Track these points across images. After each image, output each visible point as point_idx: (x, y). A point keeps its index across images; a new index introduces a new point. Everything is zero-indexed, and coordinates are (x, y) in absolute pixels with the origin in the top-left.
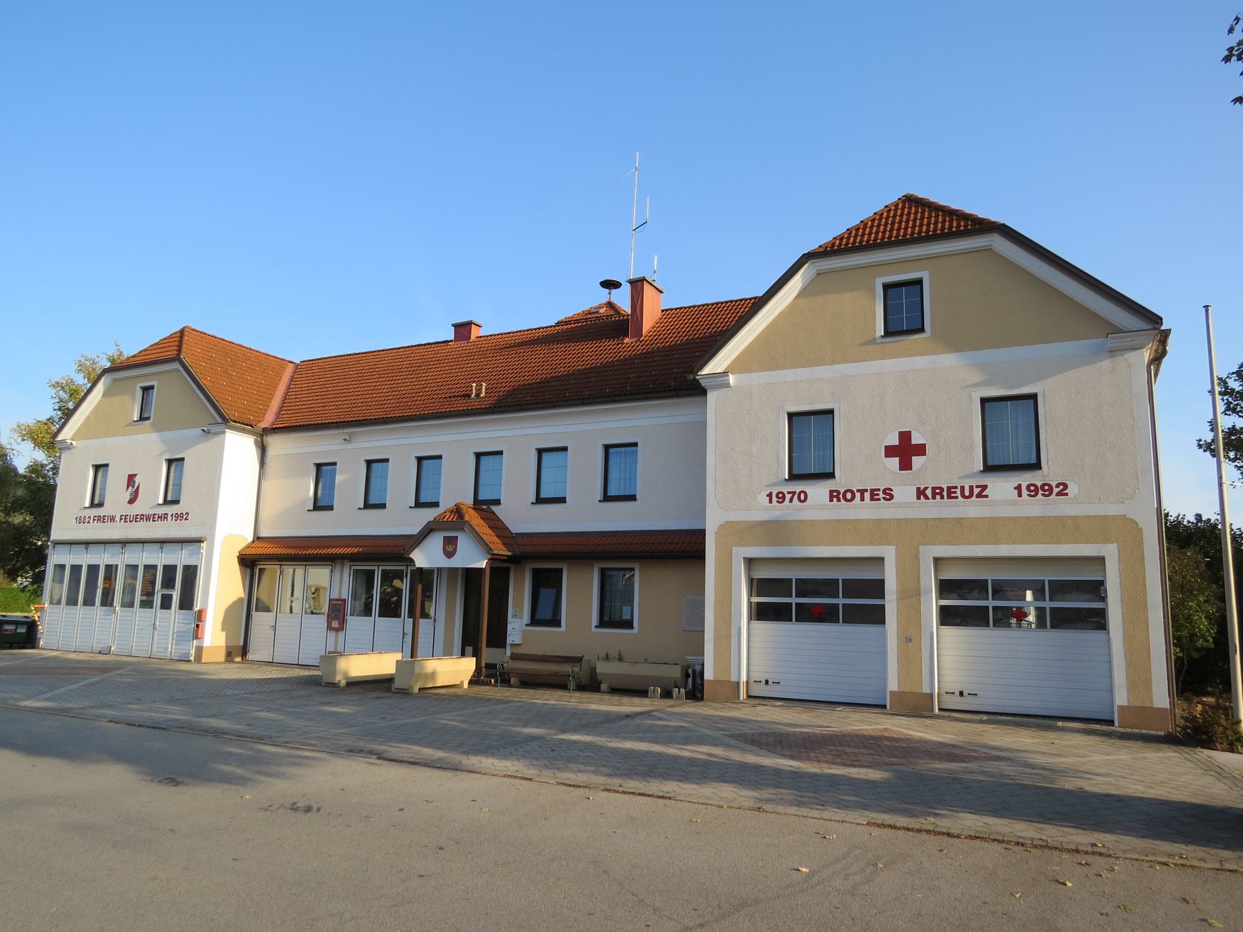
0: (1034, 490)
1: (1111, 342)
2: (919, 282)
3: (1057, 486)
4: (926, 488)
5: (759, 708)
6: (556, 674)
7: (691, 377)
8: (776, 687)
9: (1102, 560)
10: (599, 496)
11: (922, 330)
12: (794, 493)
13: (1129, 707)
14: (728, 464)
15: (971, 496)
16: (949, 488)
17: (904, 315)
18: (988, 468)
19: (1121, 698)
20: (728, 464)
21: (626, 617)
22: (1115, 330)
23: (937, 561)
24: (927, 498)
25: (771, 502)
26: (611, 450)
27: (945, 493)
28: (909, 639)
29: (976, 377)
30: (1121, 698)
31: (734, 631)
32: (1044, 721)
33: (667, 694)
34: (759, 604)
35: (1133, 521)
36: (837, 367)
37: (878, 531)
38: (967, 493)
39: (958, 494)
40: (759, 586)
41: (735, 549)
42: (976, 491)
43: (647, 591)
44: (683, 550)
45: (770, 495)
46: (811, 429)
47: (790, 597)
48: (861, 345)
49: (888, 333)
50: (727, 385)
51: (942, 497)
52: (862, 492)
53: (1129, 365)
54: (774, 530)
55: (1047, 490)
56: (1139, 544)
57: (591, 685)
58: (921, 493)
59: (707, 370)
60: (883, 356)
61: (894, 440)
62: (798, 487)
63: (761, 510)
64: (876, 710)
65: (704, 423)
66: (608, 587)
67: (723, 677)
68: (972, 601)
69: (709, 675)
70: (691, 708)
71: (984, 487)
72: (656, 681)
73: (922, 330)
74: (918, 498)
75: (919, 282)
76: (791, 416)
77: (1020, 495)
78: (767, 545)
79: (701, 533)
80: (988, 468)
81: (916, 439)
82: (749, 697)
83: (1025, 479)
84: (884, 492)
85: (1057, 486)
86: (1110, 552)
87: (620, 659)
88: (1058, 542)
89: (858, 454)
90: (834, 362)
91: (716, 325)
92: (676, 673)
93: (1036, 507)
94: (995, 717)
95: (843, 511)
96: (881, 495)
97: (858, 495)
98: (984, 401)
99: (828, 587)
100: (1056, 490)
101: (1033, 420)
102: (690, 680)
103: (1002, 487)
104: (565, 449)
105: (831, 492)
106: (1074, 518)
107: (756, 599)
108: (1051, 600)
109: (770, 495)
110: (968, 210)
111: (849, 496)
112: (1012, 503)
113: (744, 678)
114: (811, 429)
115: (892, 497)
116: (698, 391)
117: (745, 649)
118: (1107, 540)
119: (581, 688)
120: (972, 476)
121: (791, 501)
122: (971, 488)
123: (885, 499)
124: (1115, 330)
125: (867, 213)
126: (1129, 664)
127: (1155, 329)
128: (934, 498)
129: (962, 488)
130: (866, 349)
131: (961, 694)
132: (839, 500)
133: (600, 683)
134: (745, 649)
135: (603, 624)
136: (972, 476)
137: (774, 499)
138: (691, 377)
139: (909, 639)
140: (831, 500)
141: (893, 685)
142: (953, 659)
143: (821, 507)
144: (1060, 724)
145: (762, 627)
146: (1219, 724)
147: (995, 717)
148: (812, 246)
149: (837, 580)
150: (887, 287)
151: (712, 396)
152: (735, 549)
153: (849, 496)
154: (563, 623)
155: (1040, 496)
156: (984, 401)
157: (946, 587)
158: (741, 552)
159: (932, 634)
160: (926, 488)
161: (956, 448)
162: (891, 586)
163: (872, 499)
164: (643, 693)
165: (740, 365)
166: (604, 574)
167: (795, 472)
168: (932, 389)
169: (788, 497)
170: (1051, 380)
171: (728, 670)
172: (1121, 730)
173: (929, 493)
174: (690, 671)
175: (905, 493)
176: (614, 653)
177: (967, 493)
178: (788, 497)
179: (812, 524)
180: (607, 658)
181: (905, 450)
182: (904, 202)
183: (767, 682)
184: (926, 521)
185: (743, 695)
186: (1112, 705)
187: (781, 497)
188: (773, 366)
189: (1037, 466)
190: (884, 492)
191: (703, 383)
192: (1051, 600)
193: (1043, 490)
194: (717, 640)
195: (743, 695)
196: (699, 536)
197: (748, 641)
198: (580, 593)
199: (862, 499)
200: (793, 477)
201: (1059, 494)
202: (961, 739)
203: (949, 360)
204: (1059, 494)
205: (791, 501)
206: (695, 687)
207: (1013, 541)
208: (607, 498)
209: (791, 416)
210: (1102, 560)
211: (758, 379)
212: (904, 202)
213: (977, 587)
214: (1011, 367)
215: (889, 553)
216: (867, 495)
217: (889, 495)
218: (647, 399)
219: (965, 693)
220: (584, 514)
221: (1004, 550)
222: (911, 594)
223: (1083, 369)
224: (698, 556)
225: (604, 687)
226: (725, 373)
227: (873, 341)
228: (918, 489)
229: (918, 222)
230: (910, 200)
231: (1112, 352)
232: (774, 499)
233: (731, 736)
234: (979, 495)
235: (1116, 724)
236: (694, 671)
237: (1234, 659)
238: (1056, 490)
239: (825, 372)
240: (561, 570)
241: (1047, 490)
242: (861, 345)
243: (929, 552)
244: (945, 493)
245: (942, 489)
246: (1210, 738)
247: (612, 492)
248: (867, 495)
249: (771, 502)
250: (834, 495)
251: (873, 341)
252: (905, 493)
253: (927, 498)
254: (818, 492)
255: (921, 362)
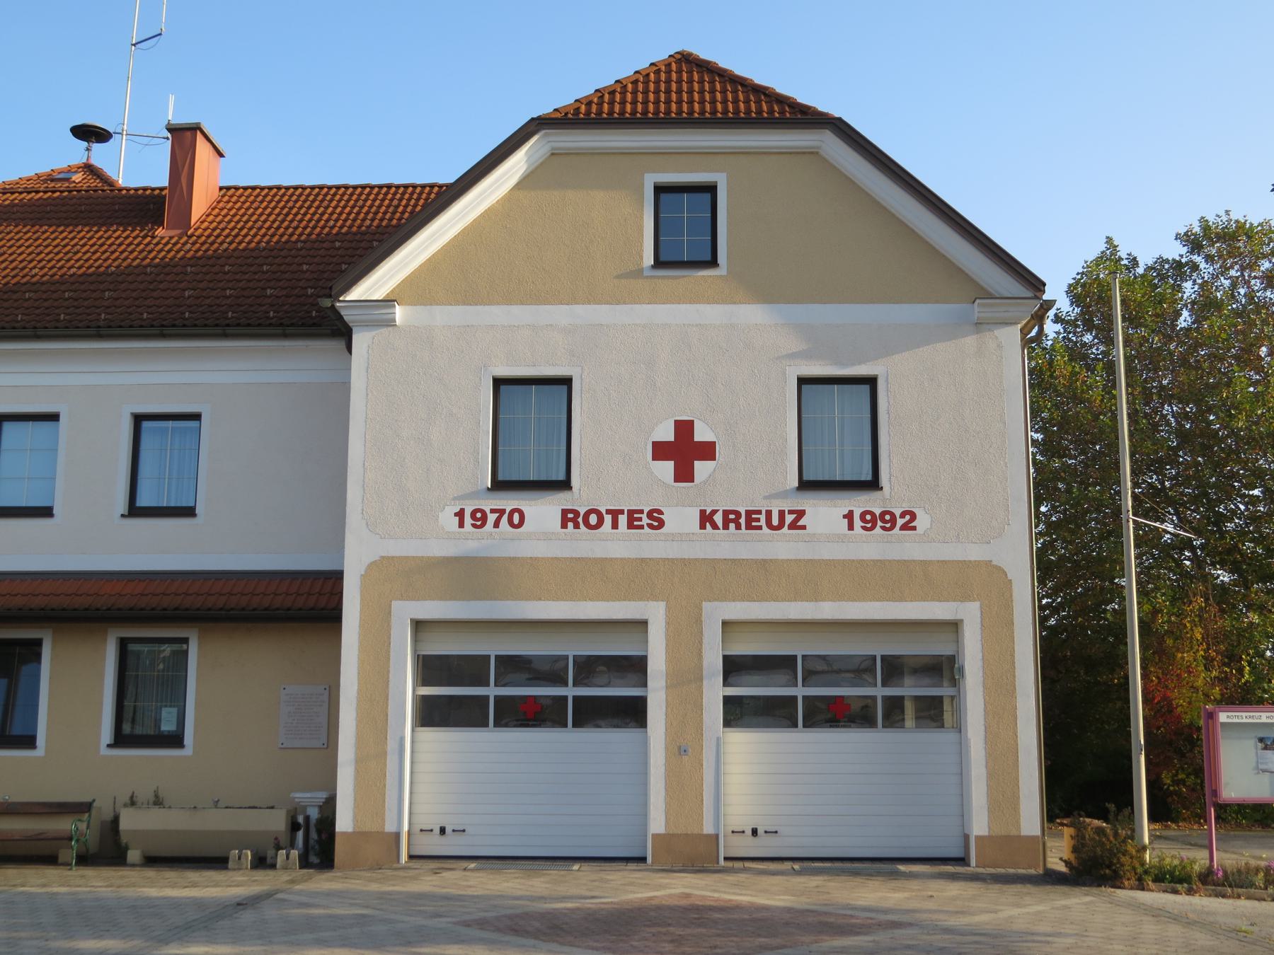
0: (870, 520)
1: (977, 310)
2: (711, 189)
3: (902, 516)
4: (714, 512)
5: (446, 874)
6: (39, 837)
7: (326, 303)
8: (771, 840)
9: (643, 624)
10: (122, 505)
11: (713, 263)
12: (502, 512)
13: (990, 837)
14: (389, 458)
15: (781, 526)
16: (749, 513)
17: (687, 237)
18: (806, 485)
19: (979, 826)
20: (389, 458)
21: (168, 726)
22: (983, 294)
23: (418, 625)
24: (715, 527)
25: (461, 525)
26: (146, 425)
27: (742, 521)
28: (684, 750)
29: (795, 345)
30: (979, 826)
31: (391, 745)
32: (883, 865)
33: (262, 862)
34: (424, 698)
35: (999, 569)
36: (579, 309)
37: (638, 577)
38: (775, 522)
39: (763, 522)
40: (431, 669)
41: (396, 605)
42: (789, 518)
43: (218, 682)
44: (303, 606)
45: (460, 514)
46: (532, 407)
47: (468, 689)
48: (618, 277)
49: (659, 263)
50: (390, 323)
51: (738, 527)
52: (615, 514)
53: (1000, 346)
54: (468, 574)
55: (887, 519)
56: (1008, 605)
57: (108, 850)
58: (706, 519)
59: (356, 294)
60: (655, 298)
61: (666, 433)
62: (508, 502)
63: (444, 538)
64: (632, 866)
65: (345, 387)
66: (130, 673)
67: (369, 826)
68: (779, 689)
69: (344, 823)
70: (322, 882)
71: (800, 514)
72: (241, 839)
73: (713, 263)
74: (703, 527)
75: (711, 189)
76: (499, 383)
77: (851, 527)
78: (441, 599)
79: (336, 578)
80: (806, 485)
81: (702, 434)
82: (411, 857)
83: (860, 502)
84: (650, 515)
85: (902, 516)
86: (970, 613)
87: (158, 802)
88: (902, 599)
89: (611, 454)
90: (573, 300)
91: (394, 214)
92: (277, 822)
93: (873, 546)
94: (808, 863)
95: (583, 544)
96: (645, 521)
97: (608, 519)
98: (802, 381)
99: (551, 672)
100: (900, 522)
101: (867, 415)
102: (300, 834)
103: (825, 514)
104: (54, 417)
105: (565, 512)
106: (925, 564)
107: (945, 691)
108: (884, 685)
109: (460, 514)
110: (782, 88)
111: (593, 519)
112: (839, 538)
113: (406, 828)
114: (532, 407)
115: (661, 524)
116: (342, 332)
117: (415, 780)
118: (966, 598)
119: (84, 860)
120: (784, 495)
121: (496, 525)
122: (782, 514)
123: (650, 526)
124: (983, 294)
125: (625, 71)
126: (991, 775)
127: (1037, 298)
128: (726, 527)
129: (769, 513)
130: (626, 284)
131: (755, 832)
132: (577, 526)
133: (126, 848)
134: (415, 780)
135: (121, 740)
136: (784, 495)
137: (468, 520)
138: (326, 303)
139: (684, 750)
140: (564, 526)
141: (657, 824)
142: (752, 778)
143: (547, 537)
144: (902, 868)
145: (434, 737)
146: (1125, 853)
147: (808, 863)
148: (545, 108)
149: (795, 657)
150: (660, 190)
151: (360, 340)
152: (396, 605)
153: (593, 519)
154: (41, 740)
155: (878, 530)
156: (802, 381)
157: (430, 669)
158: (406, 611)
159: (402, 739)
160: (714, 512)
161: (758, 453)
162: (657, 664)
163: (631, 526)
164: (220, 862)
165: (416, 289)
166: (123, 644)
167: (809, 476)
168: (706, 357)
169: (492, 518)
170: (897, 357)
171: (380, 813)
172: (980, 870)
173: (718, 518)
174: (301, 819)
175: (680, 519)
176: (145, 794)
177: (775, 522)
178: (492, 518)
179: (533, 563)
180: (132, 802)
181: (684, 451)
182: (679, 62)
183: (443, 831)
184: (713, 563)
185: (404, 857)
186: (966, 838)
187: (480, 518)
188: (470, 297)
189: (873, 484)
190: (650, 515)
191: (347, 315)
192: (884, 685)
193: (884, 521)
194: (360, 761)
195: (404, 857)
196: (328, 585)
197: (412, 763)
198: (74, 689)
199: (615, 525)
200: (499, 485)
201: (904, 527)
202: (804, 899)
203: (753, 314)
204: (904, 527)
205: (496, 525)
206: (317, 843)
207: (839, 596)
208: (134, 511)
209: (499, 383)
210: (643, 624)
211: (444, 316)
212: (679, 62)
213: (471, 670)
214: (846, 332)
215: (656, 613)
216: (623, 520)
217: (656, 519)
218: (285, 336)
219: (760, 831)
220: (89, 538)
221: (828, 610)
222: (685, 679)
223: (939, 346)
224: (330, 617)
225: (134, 855)
226: (388, 302)
227: (638, 273)
228: (703, 512)
229: (691, 94)
230: (686, 60)
231: (980, 325)
232: (468, 520)
233: (467, 924)
234: (793, 526)
235: (973, 862)
236: (307, 818)
237: (1139, 762)
238: (900, 522)
239: (561, 314)
240: (38, 643)
241: (887, 519)
242: (618, 277)
243: (717, 612)
244: (742, 521)
245: (738, 514)
246: (1115, 872)
247: (143, 501)
248: (623, 520)
249: (461, 525)
250: (569, 518)
251: (638, 273)
252: (680, 519)
253: (715, 527)
254: (542, 512)
255: (713, 313)
